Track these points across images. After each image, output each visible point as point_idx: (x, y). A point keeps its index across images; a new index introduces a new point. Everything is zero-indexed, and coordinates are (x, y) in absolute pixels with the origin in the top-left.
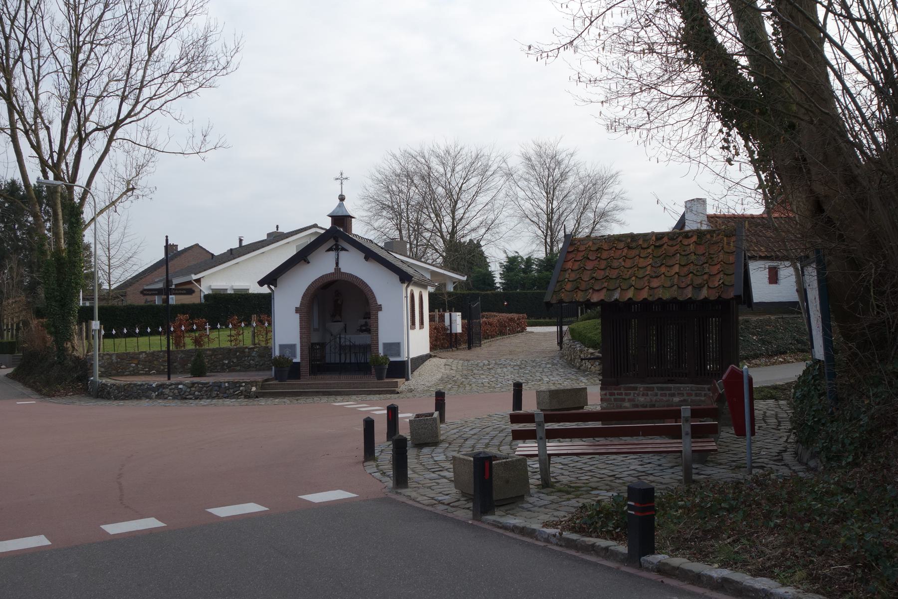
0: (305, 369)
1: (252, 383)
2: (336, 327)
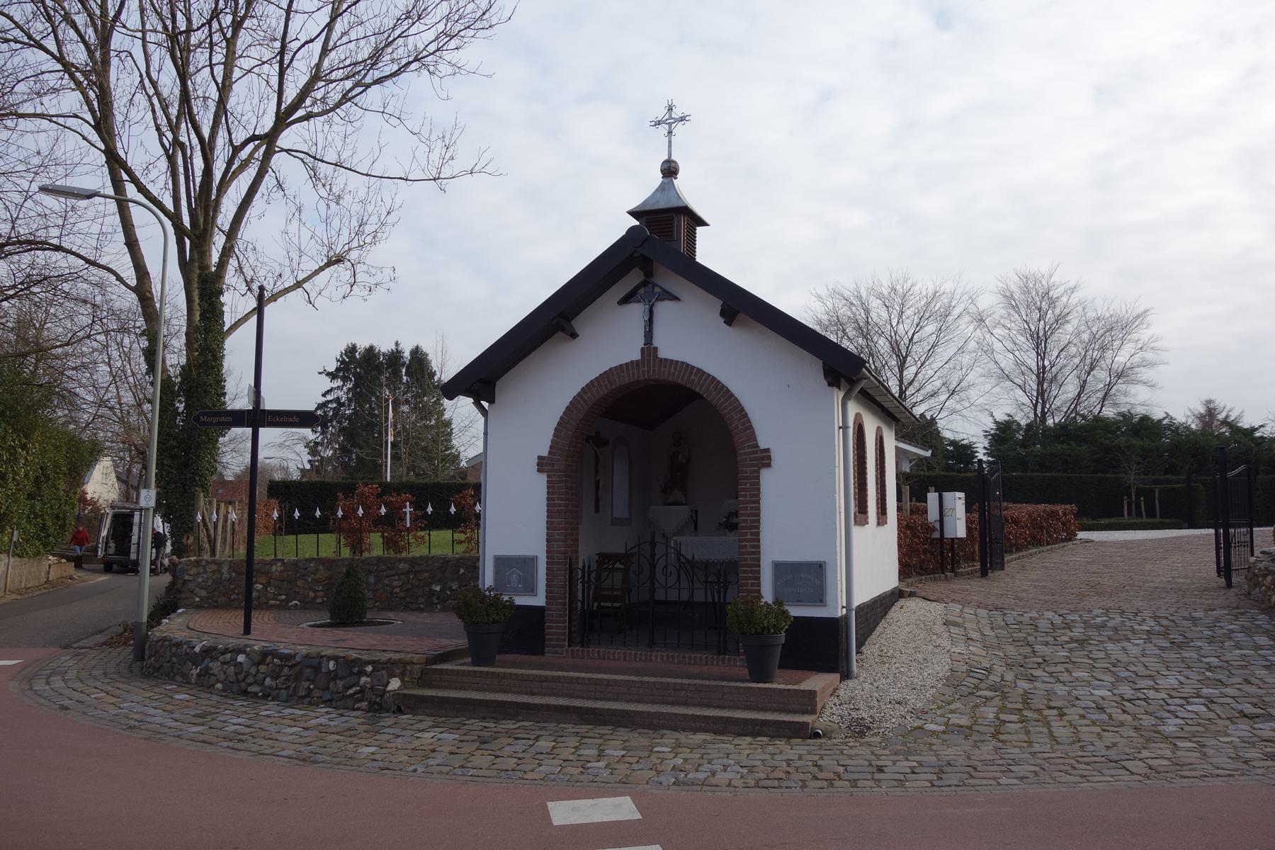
0: (556, 628)
1: (390, 668)
2: (671, 517)
